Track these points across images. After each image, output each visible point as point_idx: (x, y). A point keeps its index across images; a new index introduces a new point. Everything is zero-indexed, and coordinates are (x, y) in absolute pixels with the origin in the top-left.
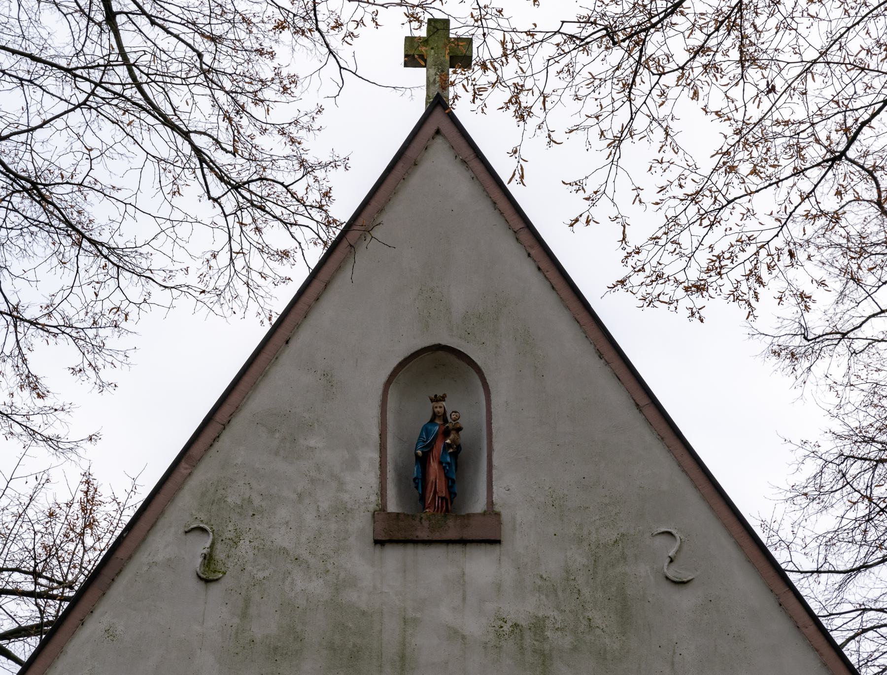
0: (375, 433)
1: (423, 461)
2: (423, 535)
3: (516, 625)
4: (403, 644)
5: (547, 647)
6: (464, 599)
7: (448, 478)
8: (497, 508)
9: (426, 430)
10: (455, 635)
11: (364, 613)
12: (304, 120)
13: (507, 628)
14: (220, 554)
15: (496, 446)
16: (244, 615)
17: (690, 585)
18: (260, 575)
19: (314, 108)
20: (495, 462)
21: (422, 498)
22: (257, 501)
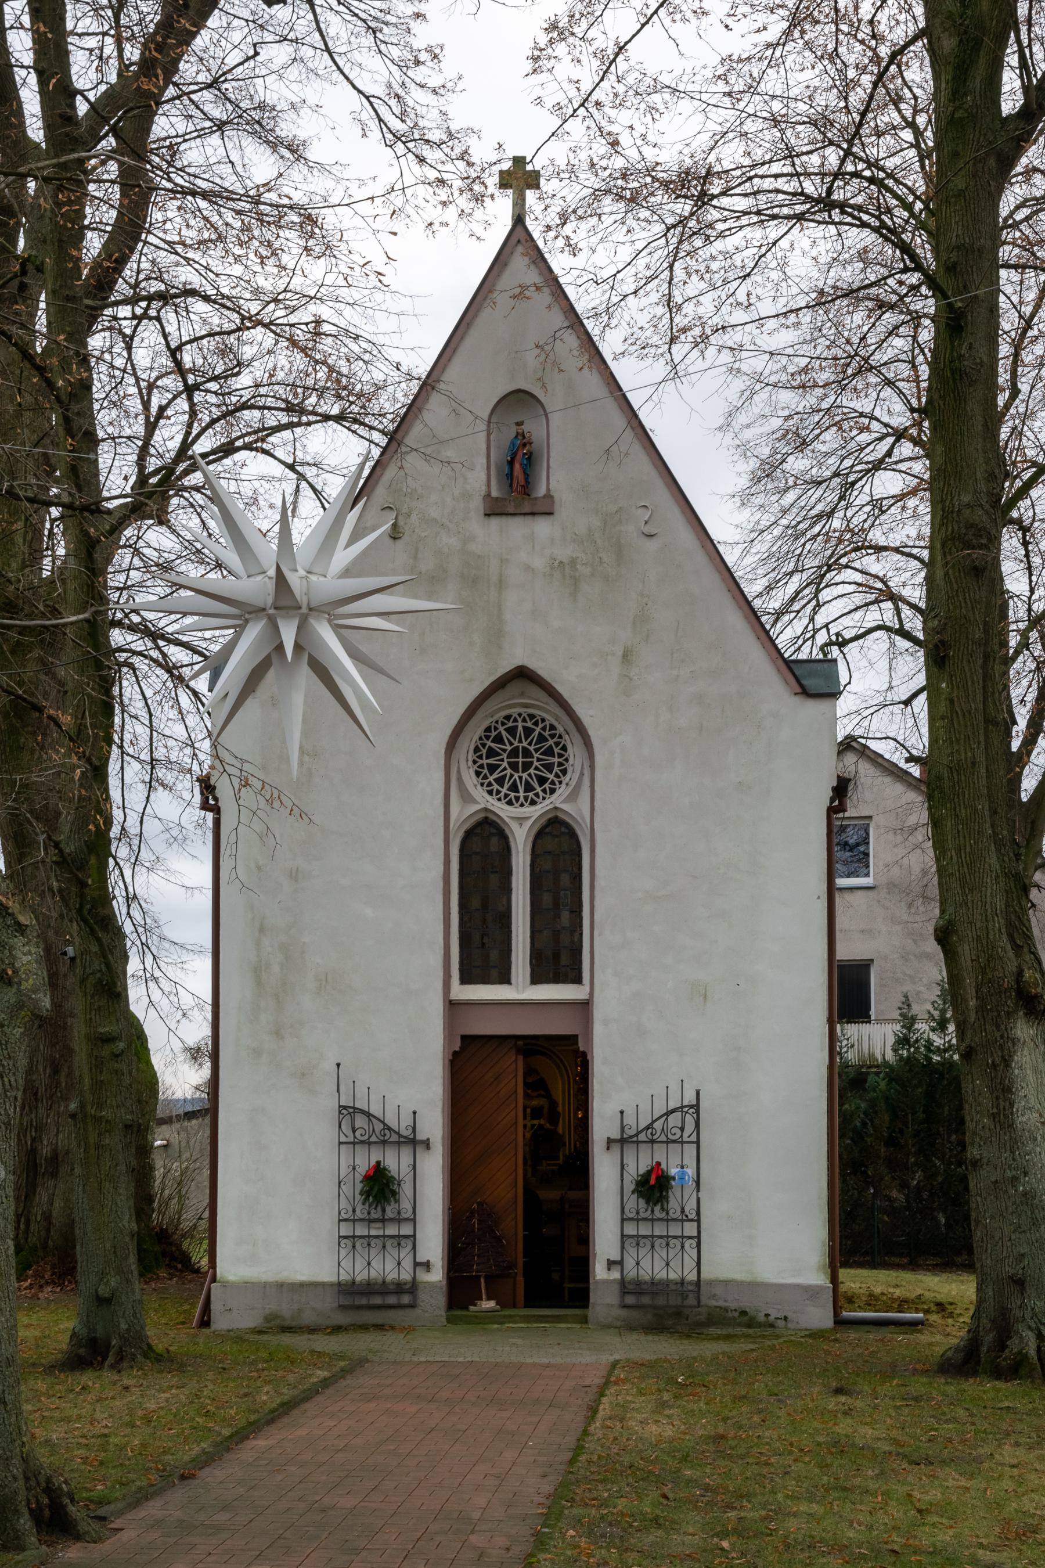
0: (484, 447)
1: (511, 463)
2: (511, 510)
3: (561, 562)
4: (501, 575)
5: (577, 574)
6: (533, 547)
7: (525, 473)
8: (552, 493)
9: (513, 443)
10: (528, 568)
11: (479, 556)
12: (449, 85)
13: (556, 564)
14: (401, 523)
15: (552, 454)
16: (415, 558)
17: (654, 538)
18: (423, 535)
19: (455, 76)
20: (551, 464)
21: (511, 485)
22: (420, 490)
